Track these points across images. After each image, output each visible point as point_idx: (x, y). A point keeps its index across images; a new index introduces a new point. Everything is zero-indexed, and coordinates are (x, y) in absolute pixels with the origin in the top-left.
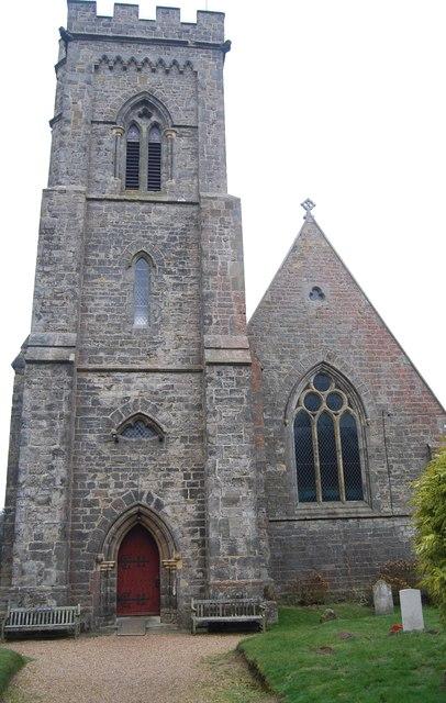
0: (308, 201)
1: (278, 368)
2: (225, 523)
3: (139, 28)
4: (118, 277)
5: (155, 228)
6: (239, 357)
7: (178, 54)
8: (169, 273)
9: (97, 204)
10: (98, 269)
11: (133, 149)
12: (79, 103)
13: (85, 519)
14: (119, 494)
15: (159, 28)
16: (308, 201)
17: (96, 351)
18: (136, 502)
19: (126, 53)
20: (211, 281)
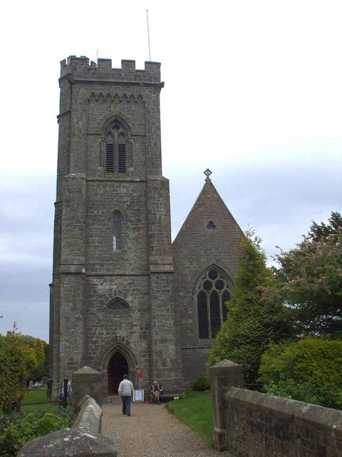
2: (160, 352)
4: (104, 224)
6: (169, 268)
11: (110, 148)
14: (109, 338)
15: (123, 75)
17: (94, 265)
19: (105, 90)
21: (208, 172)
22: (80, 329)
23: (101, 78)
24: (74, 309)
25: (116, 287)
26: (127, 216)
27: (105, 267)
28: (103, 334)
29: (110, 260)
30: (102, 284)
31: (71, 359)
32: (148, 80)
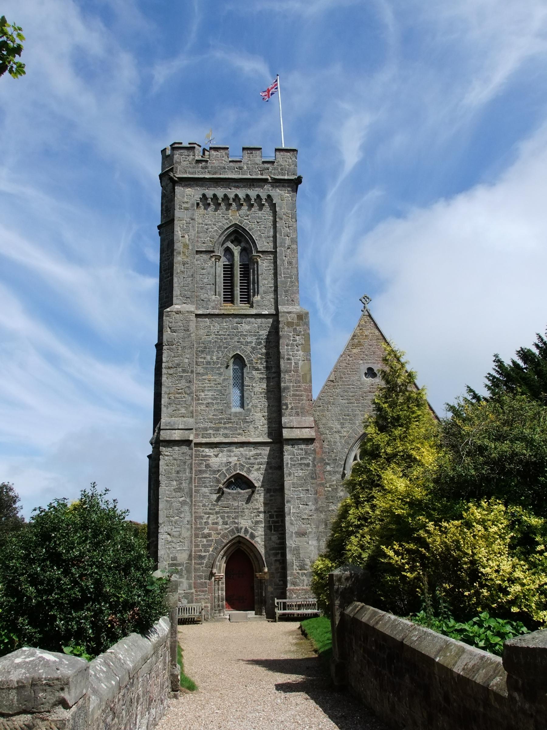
0: (366, 297)
1: (339, 432)
2: (297, 549)
3: (229, 168)
4: (220, 374)
5: (245, 335)
6: (306, 434)
7: (263, 192)
8: (257, 369)
10: (206, 368)
12: (186, 236)
13: (203, 546)
14: (226, 529)
15: (245, 168)
16: (366, 297)
17: (206, 429)
18: (237, 535)
22: (37, 714)
23: (215, 173)
24: (179, 489)
25: (236, 458)
26: (251, 362)
27: (222, 431)
29: (229, 423)
31: (174, 559)
32: (279, 174)
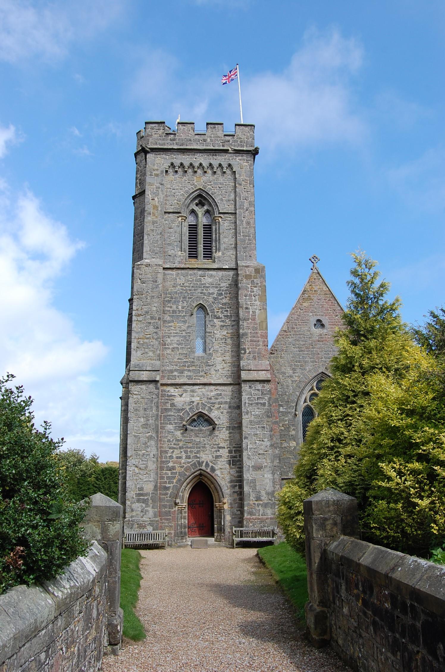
2: (254, 481)
4: (185, 322)
6: (263, 375)
9: (170, 272)
11: (193, 228)
12: (156, 199)
14: (189, 463)
17: (172, 371)
19: (187, 159)
20: (245, 324)
21: (397, 300)
22: (153, 451)
23: (182, 145)
24: (145, 426)
26: (213, 311)
27: (186, 373)
28: (180, 458)
30: (181, 396)
31: (141, 489)
32: (239, 145)
